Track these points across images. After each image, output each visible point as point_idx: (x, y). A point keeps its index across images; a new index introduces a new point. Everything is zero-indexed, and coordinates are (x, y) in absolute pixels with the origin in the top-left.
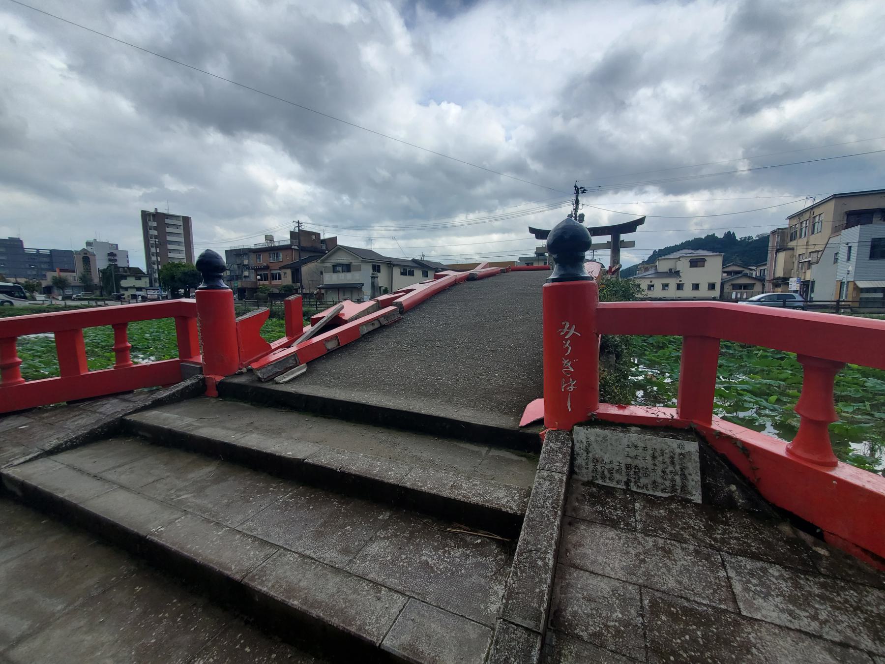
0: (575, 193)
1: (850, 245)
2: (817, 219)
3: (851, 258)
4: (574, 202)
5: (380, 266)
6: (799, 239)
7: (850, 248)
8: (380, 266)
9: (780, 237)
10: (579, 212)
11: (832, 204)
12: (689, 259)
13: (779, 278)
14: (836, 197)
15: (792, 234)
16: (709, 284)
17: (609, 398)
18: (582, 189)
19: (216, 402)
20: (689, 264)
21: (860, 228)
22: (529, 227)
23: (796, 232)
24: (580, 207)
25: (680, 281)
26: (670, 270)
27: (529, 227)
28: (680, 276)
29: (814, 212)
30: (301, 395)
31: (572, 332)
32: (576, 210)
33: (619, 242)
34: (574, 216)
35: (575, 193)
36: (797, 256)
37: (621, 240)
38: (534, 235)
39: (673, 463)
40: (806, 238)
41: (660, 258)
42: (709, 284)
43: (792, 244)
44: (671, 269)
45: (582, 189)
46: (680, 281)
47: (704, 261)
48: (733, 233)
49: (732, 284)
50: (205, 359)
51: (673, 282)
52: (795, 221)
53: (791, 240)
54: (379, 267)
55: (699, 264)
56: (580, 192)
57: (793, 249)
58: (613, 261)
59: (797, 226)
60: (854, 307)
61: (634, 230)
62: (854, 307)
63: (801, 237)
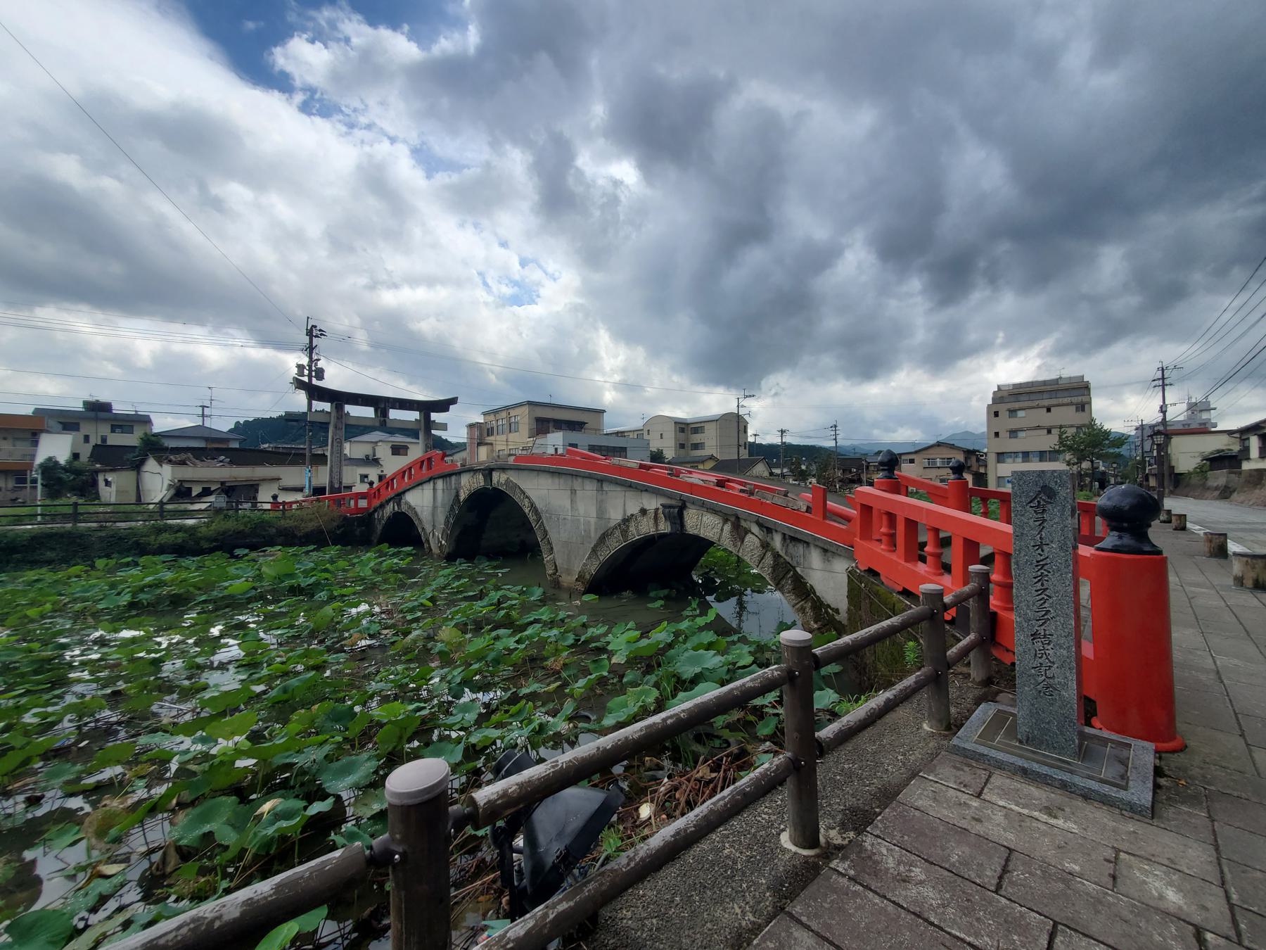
2: (513, 420)
12: (390, 444)
14: (530, 403)
15: (488, 429)
16: (680, 444)
17: (834, 919)
19: (457, 496)
20: (390, 451)
25: (382, 471)
26: (367, 457)
30: (821, 448)
41: (352, 439)
42: (680, 444)
43: (490, 439)
46: (382, 471)
47: (407, 448)
52: (492, 417)
53: (488, 435)
55: (401, 451)
57: (492, 444)
60: (48, 905)
61: (447, 410)
62: (48, 905)
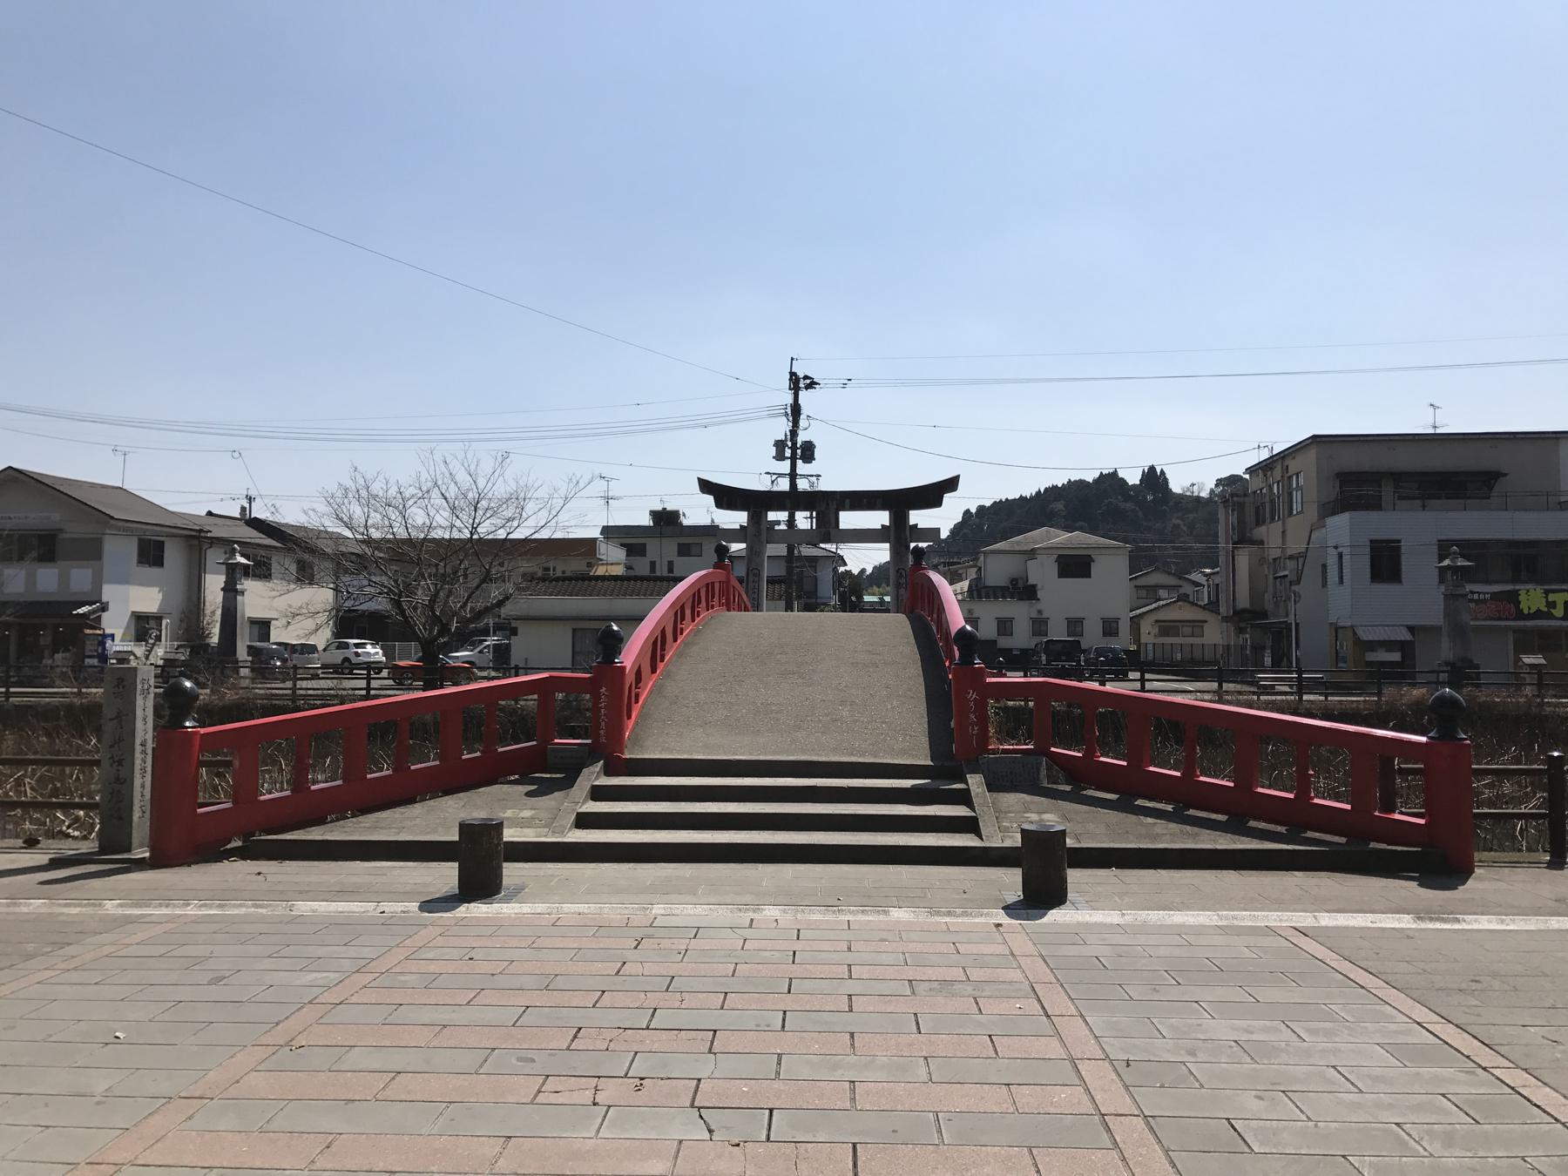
0: (790, 389)
1: (1340, 550)
3: (1328, 583)
4: (789, 411)
5: (163, 542)
6: (1270, 523)
7: (1340, 556)
8: (163, 542)
9: (1236, 513)
10: (802, 437)
11: (1312, 454)
13: (1244, 611)
18: (808, 381)
20: (1054, 569)
21: (1350, 518)
22: (699, 479)
23: (1263, 504)
24: (803, 423)
26: (1014, 581)
27: (699, 479)
28: (1039, 600)
29: (1287, 466)
31: (974, 696)
32: (794, 433)
33: (908, 528)
34: (789, 444)
35: (790, 389)
36: (1271, 561)
37: (911, 524)
38: (710, 499)
39: (1033, 768)
40: (1280, 523)
44: (1016, 580)
45: (808, 381)
48: (1162, 471)
49: (1157, 621)
50: (100, 799)
51: (1019, 612)
54: (160, 546)
56: (802, 385)
58: (897, 571)
59: (1264, 491)
63: (1273, 519)
